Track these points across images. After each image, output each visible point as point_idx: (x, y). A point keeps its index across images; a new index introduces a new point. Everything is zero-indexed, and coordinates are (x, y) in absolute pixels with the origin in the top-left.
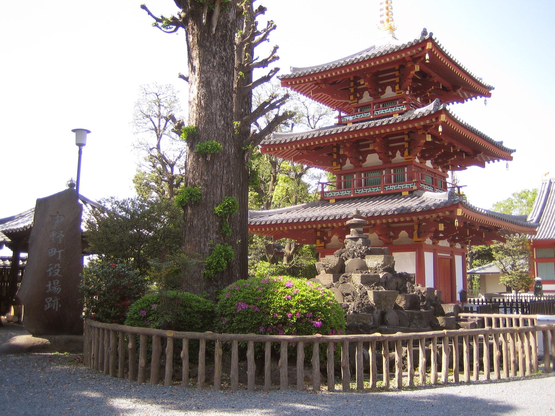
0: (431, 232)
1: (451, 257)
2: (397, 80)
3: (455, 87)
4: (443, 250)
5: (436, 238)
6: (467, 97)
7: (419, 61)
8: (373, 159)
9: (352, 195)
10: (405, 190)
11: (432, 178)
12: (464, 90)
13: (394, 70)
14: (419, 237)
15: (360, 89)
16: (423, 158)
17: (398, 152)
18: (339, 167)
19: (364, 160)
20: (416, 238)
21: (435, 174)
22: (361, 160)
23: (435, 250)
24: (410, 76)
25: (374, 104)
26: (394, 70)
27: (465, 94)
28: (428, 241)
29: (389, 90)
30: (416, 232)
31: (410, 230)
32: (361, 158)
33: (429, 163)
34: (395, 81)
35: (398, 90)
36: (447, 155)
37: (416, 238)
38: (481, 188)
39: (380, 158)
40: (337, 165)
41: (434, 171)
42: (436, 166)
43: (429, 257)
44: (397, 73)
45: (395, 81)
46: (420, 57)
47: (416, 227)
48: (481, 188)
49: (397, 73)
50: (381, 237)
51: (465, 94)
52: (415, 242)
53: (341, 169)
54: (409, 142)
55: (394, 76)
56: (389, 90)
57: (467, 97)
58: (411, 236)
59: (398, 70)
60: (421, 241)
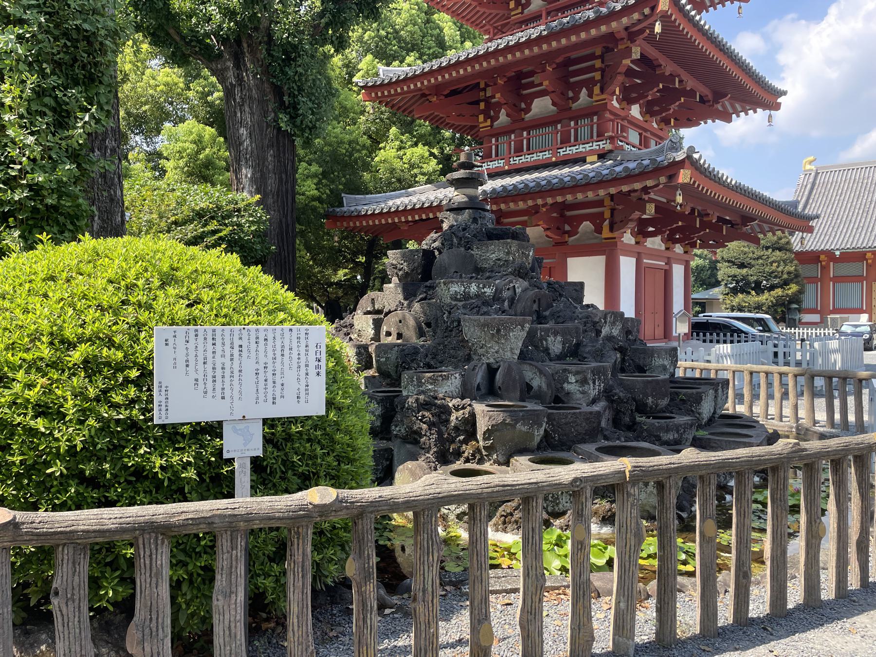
0: (631, 220)
1: (667, 267)
2: (597, 75)
3: (719, 96)
4: (654, 254)
5: (642, 233)
6: (739, 109)
7: (641, 37)
8: (542, 106)
9: (506, 167)
10: (591, 153)
11: (640, 134)
12: (734, 99)
13: (592, 57)
14: (611, 230)
15: (527, 95)
16: (627, 99)
17: (584, 90)
18: (489, 123)
19: (528, 110)
20: (606, 233)
21: (646, 130)
22: (523, 110)
23: (639, 253)
24: (622, 69)
25: (548, 14)
26: (592, 57)
27: (737, 105)
28: (628, 238)
29: (586, 226)
30: (607, 223)
31: (597, 221)
32: (523, 106)
33: (635, 111)
34: (594, 77)
35: (597, 95)
36: (670, 94)
37: (606, 233)
38: (725, 147)
39: (554, 104)
40: (485, 120)
41: (645, 125)
42: (648, 117)
43: (627, 266)
44: (598, 63)
45: (594, 77)
46: (642, 31)
47: (607, 215)
48: (725, 147)
49: (598, 63)
50: (549, 233)
51: (737, 105)
52: (606, 239)
53: (492, 126)
54: (603, 71)
55: (592, 69)
56: (586, 226)
57: (739, 109)
58: (599, 230)
59: (602, 57)
60: (614, 238)
